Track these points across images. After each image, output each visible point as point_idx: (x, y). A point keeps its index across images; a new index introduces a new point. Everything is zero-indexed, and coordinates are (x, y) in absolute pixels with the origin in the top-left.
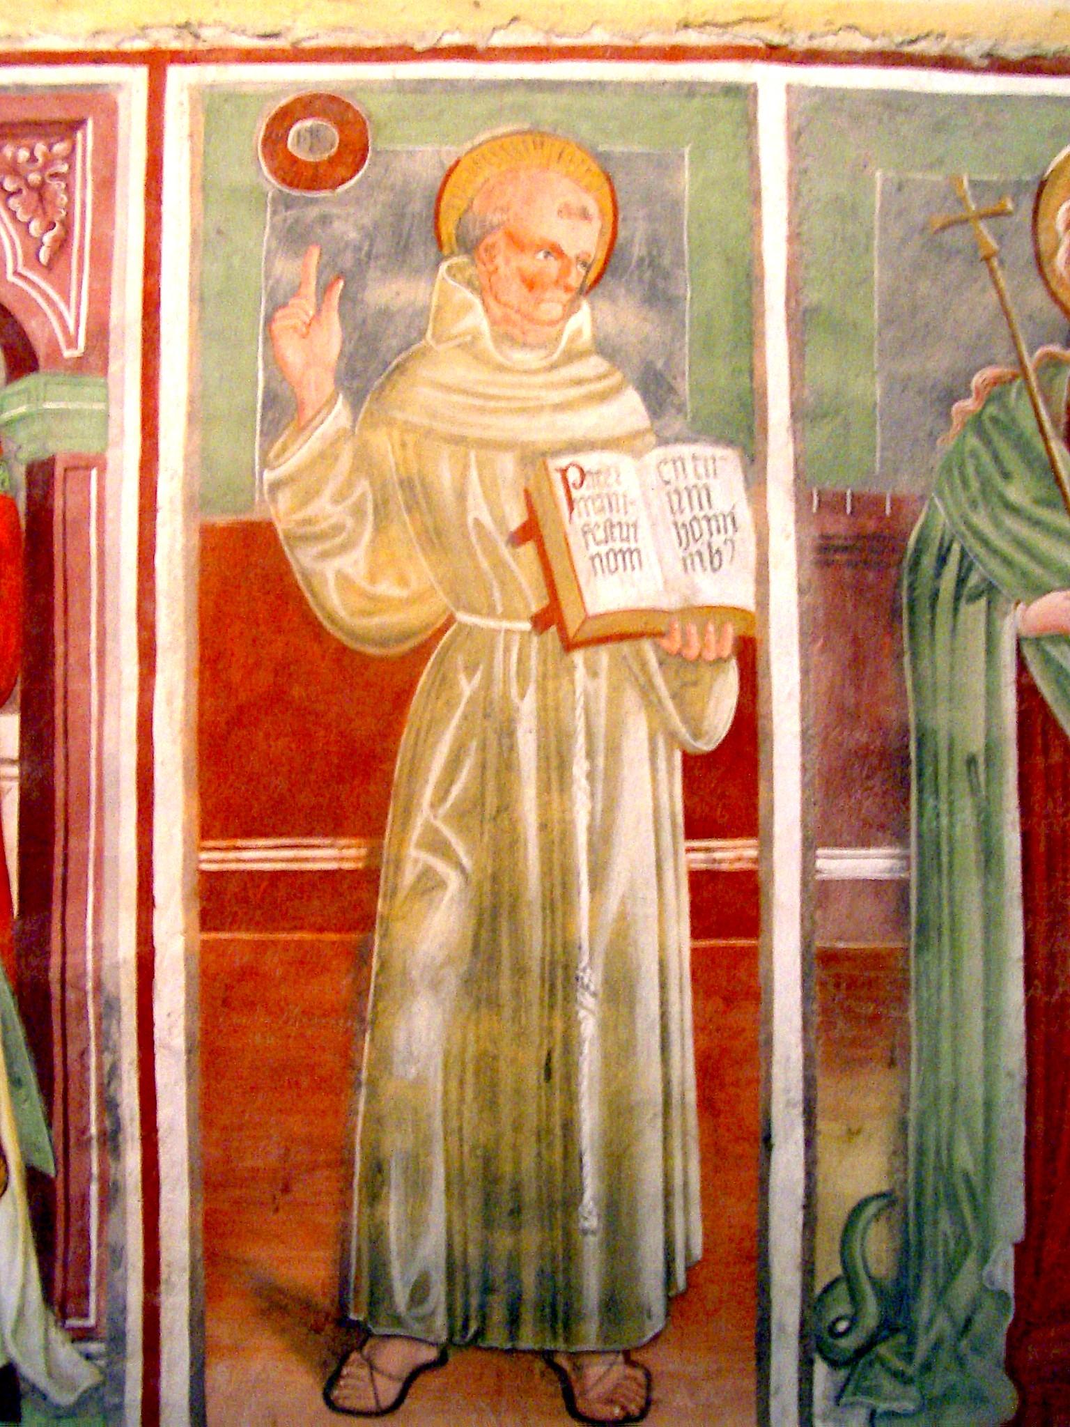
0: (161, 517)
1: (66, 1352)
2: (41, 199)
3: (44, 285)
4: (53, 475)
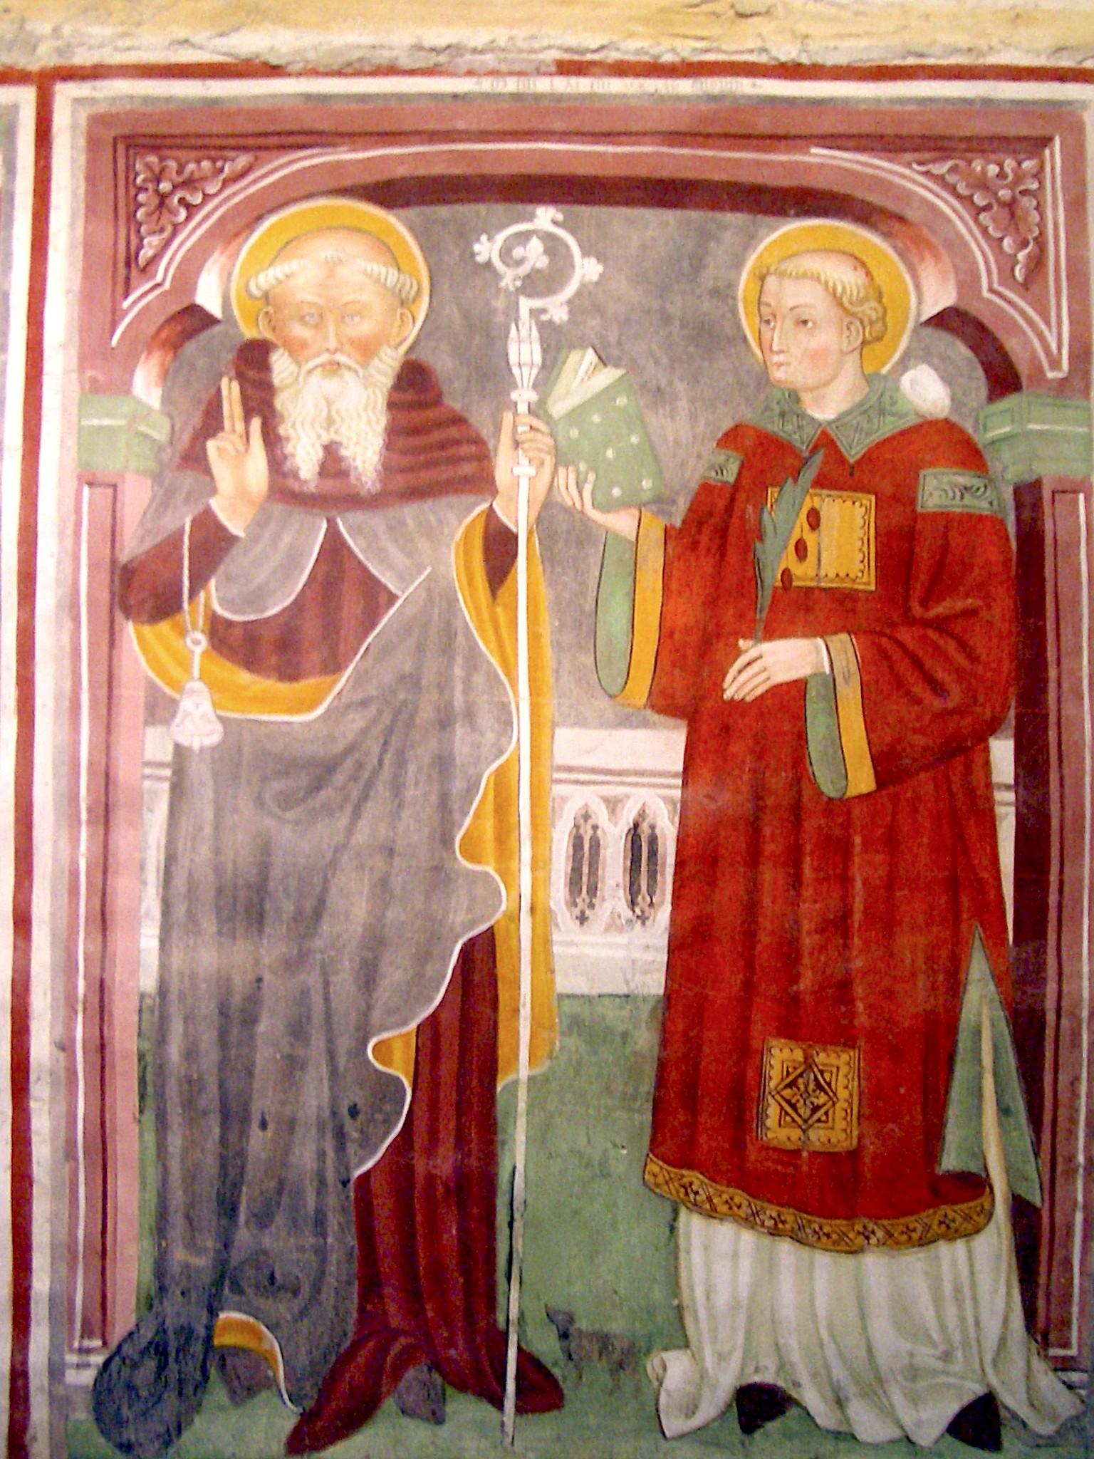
0: (46, 380)
1: (1047, 1381)
2: (1013, 215)
3: (1022, 304)
4: (1041, 499)
